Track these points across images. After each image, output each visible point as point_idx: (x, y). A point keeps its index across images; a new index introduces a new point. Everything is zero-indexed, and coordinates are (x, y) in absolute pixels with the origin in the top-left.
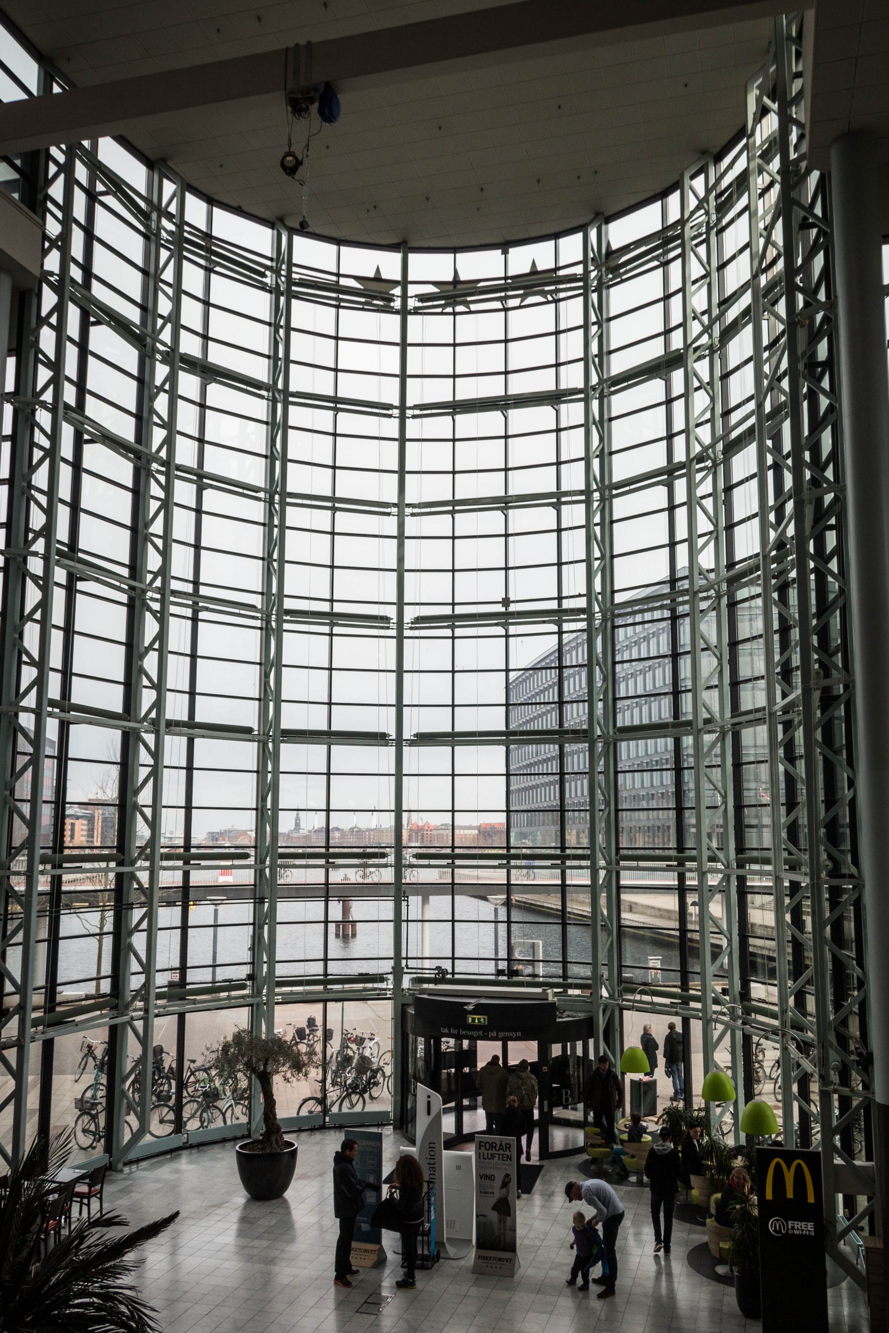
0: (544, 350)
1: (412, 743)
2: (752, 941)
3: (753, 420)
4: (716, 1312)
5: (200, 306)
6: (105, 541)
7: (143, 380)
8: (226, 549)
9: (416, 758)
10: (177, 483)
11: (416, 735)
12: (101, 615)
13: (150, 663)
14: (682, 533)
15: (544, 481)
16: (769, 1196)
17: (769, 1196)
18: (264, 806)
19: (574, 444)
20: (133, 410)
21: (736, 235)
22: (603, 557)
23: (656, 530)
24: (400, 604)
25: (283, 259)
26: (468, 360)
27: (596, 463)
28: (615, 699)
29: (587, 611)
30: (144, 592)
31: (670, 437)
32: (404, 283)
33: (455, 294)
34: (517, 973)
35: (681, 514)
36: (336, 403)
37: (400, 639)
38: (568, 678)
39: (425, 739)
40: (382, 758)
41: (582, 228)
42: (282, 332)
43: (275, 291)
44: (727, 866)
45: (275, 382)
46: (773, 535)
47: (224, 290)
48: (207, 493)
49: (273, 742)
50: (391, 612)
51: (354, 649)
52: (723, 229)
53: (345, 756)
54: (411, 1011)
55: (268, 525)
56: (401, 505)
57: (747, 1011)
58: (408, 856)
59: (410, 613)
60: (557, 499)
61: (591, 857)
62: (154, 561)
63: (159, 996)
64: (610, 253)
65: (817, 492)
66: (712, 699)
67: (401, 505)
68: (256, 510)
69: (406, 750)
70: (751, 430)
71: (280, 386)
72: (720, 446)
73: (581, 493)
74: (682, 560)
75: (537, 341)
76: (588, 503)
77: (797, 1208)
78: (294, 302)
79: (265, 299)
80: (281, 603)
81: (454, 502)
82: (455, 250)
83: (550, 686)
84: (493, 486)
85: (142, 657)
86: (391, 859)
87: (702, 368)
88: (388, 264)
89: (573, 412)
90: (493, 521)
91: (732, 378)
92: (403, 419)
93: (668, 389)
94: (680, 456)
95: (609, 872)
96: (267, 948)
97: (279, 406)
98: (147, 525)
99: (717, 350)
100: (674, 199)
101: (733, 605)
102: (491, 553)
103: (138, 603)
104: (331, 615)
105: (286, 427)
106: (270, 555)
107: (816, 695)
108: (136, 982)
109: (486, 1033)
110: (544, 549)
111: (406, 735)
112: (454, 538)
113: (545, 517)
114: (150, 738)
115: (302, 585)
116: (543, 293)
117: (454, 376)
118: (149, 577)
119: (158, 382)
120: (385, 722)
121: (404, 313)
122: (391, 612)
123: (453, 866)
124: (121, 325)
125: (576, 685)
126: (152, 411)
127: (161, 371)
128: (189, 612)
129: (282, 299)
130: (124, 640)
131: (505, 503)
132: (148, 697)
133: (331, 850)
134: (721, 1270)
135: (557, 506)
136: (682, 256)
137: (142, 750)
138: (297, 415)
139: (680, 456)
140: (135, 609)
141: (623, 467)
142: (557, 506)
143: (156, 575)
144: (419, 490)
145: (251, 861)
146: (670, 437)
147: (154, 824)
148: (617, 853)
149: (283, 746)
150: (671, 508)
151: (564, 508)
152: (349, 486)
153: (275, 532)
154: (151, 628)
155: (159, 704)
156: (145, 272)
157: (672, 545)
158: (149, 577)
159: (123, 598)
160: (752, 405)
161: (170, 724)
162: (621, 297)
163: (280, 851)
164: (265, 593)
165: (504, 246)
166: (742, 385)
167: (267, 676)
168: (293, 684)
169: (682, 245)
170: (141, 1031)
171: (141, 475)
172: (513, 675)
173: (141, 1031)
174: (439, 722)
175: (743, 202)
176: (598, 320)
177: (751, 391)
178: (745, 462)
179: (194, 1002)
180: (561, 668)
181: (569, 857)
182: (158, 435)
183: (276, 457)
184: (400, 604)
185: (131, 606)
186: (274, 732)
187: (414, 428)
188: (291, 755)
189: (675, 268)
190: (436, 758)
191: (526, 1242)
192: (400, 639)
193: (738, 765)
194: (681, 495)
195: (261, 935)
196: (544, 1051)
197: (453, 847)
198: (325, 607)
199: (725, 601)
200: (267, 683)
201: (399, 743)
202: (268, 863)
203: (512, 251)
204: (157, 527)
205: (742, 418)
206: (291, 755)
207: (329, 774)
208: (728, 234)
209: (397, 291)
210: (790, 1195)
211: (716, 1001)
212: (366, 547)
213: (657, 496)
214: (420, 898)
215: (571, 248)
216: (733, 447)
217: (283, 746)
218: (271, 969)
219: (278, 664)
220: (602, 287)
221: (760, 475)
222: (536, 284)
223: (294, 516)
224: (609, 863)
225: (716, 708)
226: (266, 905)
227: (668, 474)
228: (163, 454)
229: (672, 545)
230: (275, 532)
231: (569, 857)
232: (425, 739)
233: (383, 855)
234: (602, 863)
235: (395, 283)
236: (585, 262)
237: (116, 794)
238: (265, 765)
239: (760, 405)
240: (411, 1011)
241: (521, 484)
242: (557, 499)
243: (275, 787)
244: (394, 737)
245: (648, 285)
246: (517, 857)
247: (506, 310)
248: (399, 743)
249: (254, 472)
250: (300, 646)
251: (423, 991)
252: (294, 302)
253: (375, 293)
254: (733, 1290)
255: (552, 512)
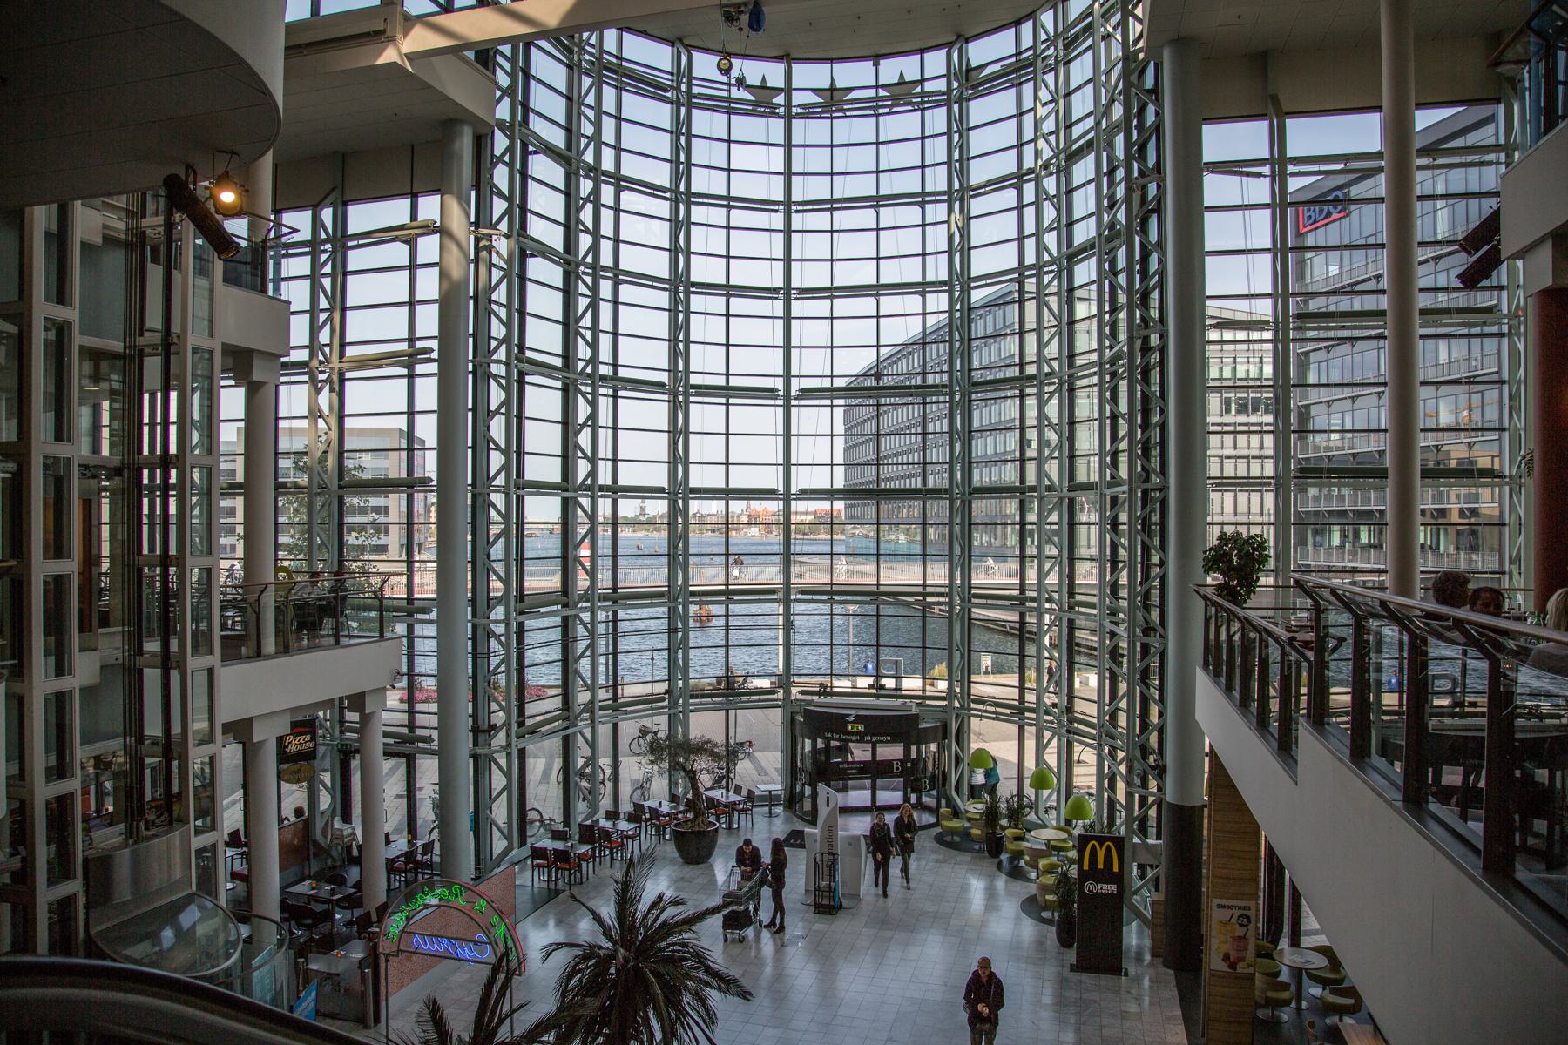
0: (910, 155)
2: (1078, 633)
3: (1092, 134)
4: (1040, 943)
5: (613, 121)
6: (544, 338)
7: (569, 193)
8: (642, 235)
10: (603, 186)
12: (543, 400)
13: (584, 439)
14: (1030, 228)
15: (910, 183)
16: (1086, 867)
17: (1086, 867)
19: (938, 150)
20: (561, 220)
21: (1081, 69)
22: (961, 248)
23: (1007, 226)
24: (787, 376)
25: (683, 74)
26: (843, 160)
27: (956, 137)
28: (970, 340)
29: (950, 386)
30: (578, 266)
31: (1020, 145)
32: (788, 90)
33: (833, 102)
34: (882, 687)
35: (1030, 213)
36: (729, 202)
37: (787, 409)
41: (948, 45)
42: (683, 139)
43: (675, 103)
44: (1061, 609)
45: (678, 186)
46: (1106, 218)
47: (635, 106)
48: (625, 195)
50: (779, 384)
51: (747, 416)
52: (1069, 62)
54: (800, 719)
55: (673, 311)
56: (788, 202)
57: (1071, 721)
59: (795, 386)
60: (922, 199)
62: (584, 352)
63: (602, 708)
64: (969, 70)
65: (1145, 332)
66: (1053, 468)
67: (788, 202)
68: (662, 299)
70: (1090, 143)
71: (682, 188)
72: (1063, 156)
73: (943, 193)
74: (1032, 577)
75: (905, 146)
76: (951, 292)
77: (1107, 876)
78: (694, 111)
79: (666, 109)
80: (687, 379)
81: (832, 201)
82: (832, 61)
84: (865, 186)
85: (577, 433)
87: (1050, 184)
88: (774, 73)
89: (937, 212)
90: (866, 217)
91: (1074, 96)
92: (787, 602)
93: (1020, 196)
94: (1029, 162)
97: (682, 207)
98: (578, 320)
99: (1065, 172)
100: (1027, 27)
101: (1072, 390)
102: (864, 245)
103: (571, 388)
104: (727, 388)
105: (688, 223)
106: (676, 339)
107: (1138, 343)
108: (583, 697)
109: (860, 738)
110: (910, 241)
111: (793, 490)
112: (832, 174)
113: (912, 214)
114: (585, 502)
115: (705, 363)
116: (912, 104)
117: (832, 146)
118: (581, 365)
119: (581, 420)
121: (789, 118)
122: (779, 384)
124: (550, 150)
125: (938, 454)
126: (578, 221)
127: (586, 186)
128: (610, 392)
129: (683, 110)
130: (560, 352)
131: (876, 202)
132: (583, 468)
134: (1045, 914)
135: (922, 205)
136: (1034, 79)
137: (580, 571)
138: (698, 213)
139: (1029, 162)
140: (568, 393)
141: (980, 172)
142: (922, 205)
143: (588, 362)
144: (804, 276)
146: (1020, 145)
147: (592, 574)
150: (1021, 207)
151: (928, 207)
152: (743, 274)
153: (680, 225)
154: (583, 411)
155: (593, 474)
156: (569, 99)
157: (1021, 239)
158: (581, 365)
159: (559, 384)
160: (1090, 122)
161: (601, 488)
162: (980, 110)
164: (672, 370)
165: (876, 58)
166: (1082, 103)
167: (676, 444)
168: (699, 448)
169: (1034, 72)
170: (589, 736)
171: (570, 277)
172: (883, 351)
173: (589, 338)
175: (1090, 42)
176: (959, 129)
177: (1092, 208)
178: (1084, 170)
179: (626, 713)
182: (585, 241)
183: (679, 250)
184: (787, 376)
185: (565, 390)
187: (797, 221)
189: (1028, 89)
192: (787, 409)
193: (1072, 457)
194: (1029, 196)
195: (676, 659)
196: (907, 752)
198: (721, 381)
199: (1066, 387)
200: (676, 449)
203: (882, 62)
204: (587, 321)
205: (1084, 232)
207: (727, 464)
208: (1075, 65)
209: (780, 99)
210: (1101, 866)
211: (1047, 713)
212: (757, 326)
213: (1009, 197)
215: (936, 62)
216: (1074, 156)
219: (686, 432)
220: (961, 100)
221: (1097, 180)
222: (903, 95)
223: (697, 302)
224: (962, 600)
225: (1055, 476)
227: (1017, 179)
228: (589, 260)
229: (1021, 239)
230: (680, 225)
234: (957, 598)
235: (780, 90)
236: (948, 75)
237: (559, 514)
239: (1098, 123)
240: (800, 719)
241: (890, 185)
242: (922, 199)
243: (685, 537)
245: (1002, 102)
247: (878, 116)
249: (661, 175)
250: (704, 415)
251: (810, 703)
252: (694, 111)
253: (762, 102)
254: (1054, 929)
255: (917, 209)
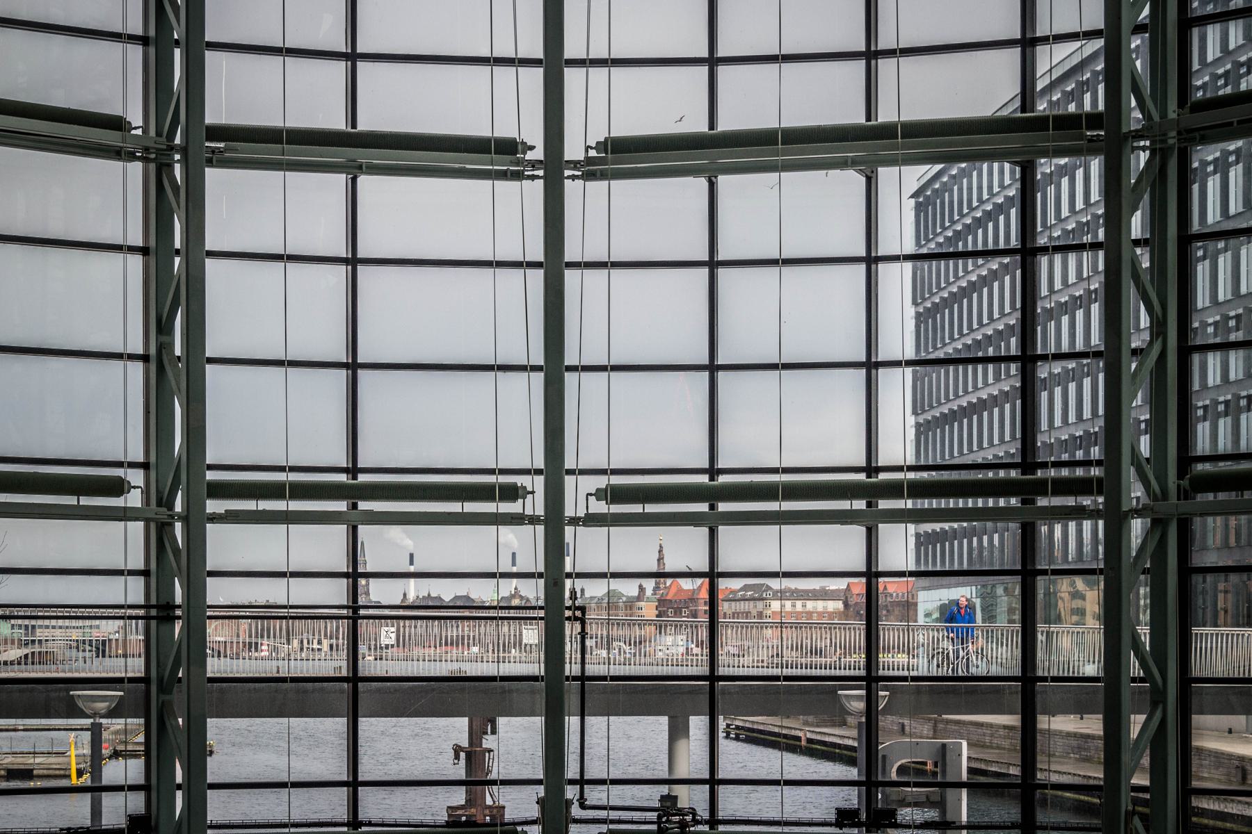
1: (591, 170)
9: (606, 215)
11: (602, 146)
18: (164, 347)
38: (1048, 384)
39: (626, 156)
40: (502, 214)
49: (185, 161)
53: (403, 209)
58: (579, 495)
61: (1110, 486)
69: (572, 189)
83: (999, 208)
86: (536, 505)
95: (1158, 524)
96: (182, 740)
111: (573, 150)
120: (513, 108)
123: (712, 523)
133: (363, 478)
145: (134, 499)
148: (1181, 474)
149: (213, 176)
163: (211, 476)
174: (670, 105)
180: (1028, 360)
181: (1041, 488)
186: (186, 135)
188: (238, 205)
190: (661, 211)
191: (366, 734)
197: (713, 472)
201: (554, 169)
202: (178, 507)
206: (238, 205)
214: (664, 720)
217: (213, 176)
218: (196, 805)
226: (178, 626)
231: (1041, 488)
232: (626, 156)
233: (511, 493)
238: (164, 230)
244: (538, 154)
246: (894, 490)
248: (554, 169)
